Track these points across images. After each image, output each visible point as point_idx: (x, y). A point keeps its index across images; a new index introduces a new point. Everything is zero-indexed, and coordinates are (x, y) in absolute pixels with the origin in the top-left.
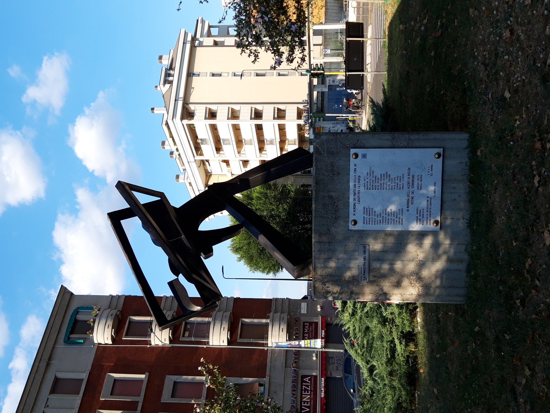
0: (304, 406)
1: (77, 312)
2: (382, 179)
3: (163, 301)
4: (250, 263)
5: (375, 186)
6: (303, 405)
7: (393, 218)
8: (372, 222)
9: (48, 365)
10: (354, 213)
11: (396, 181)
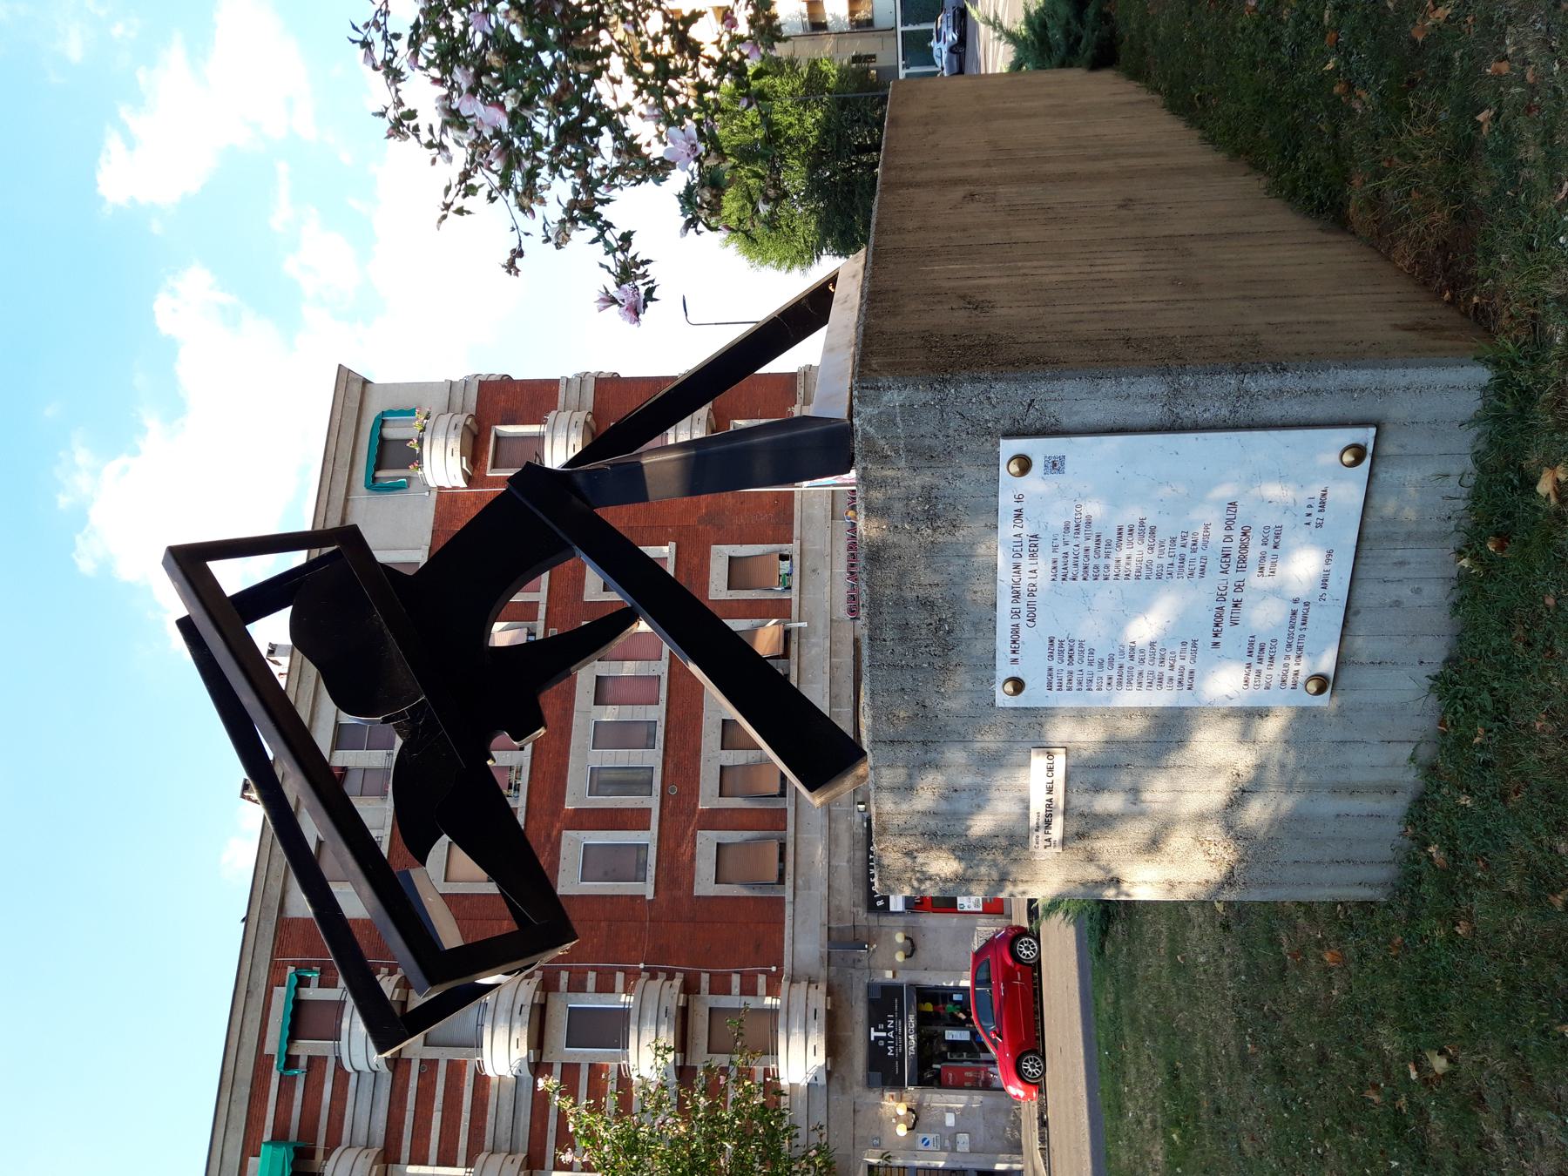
1: (381, 422)
3: (562, 388)
4: (748, 251)
5: (1096, 567)
8: (1080, 683)
10: (1014, 656)
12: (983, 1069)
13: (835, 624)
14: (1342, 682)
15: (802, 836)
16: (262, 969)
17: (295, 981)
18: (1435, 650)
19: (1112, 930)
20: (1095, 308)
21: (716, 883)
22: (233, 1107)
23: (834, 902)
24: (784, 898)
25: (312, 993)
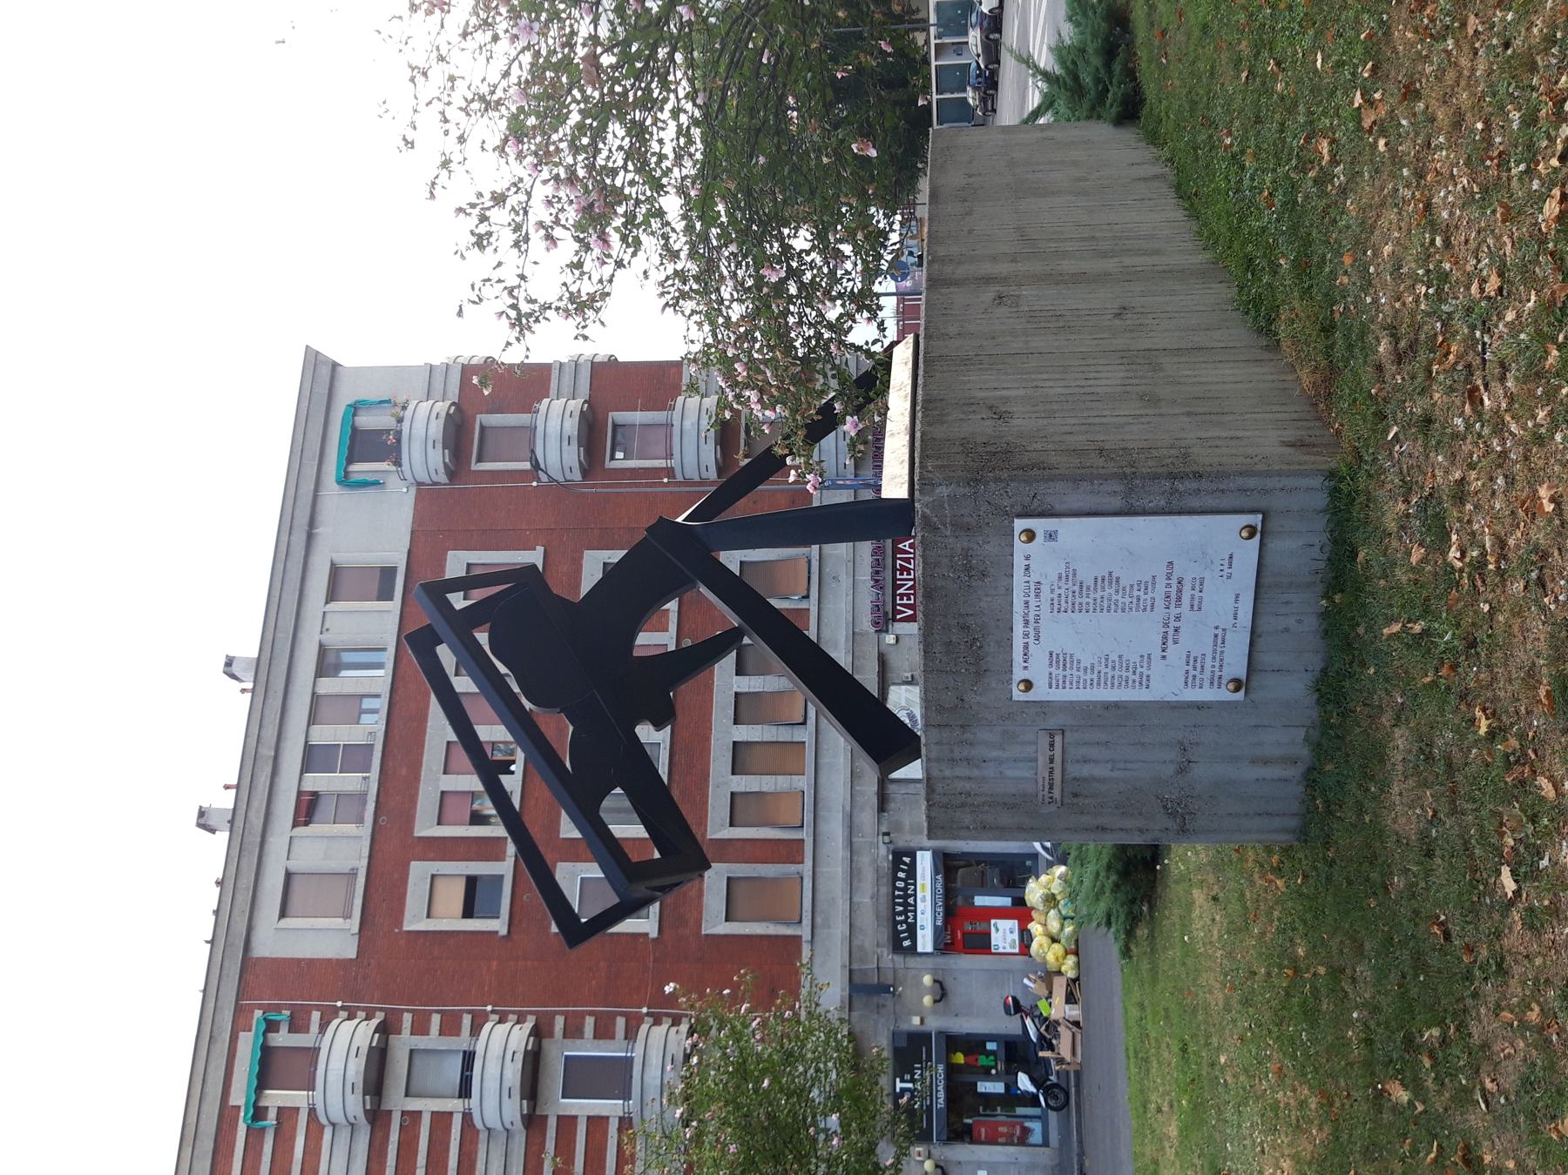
0: (901, 605)
2: (1099, 587)
5: (1081, 604)
6: (898, 602)
7: (1124, 674)
8: (1071, 683)
9: (310, 537)
10: (1026, 665)
11: (1136, 593)
12: (1018, 1123)
13: (857, 637)
14: (1254, 684)
15: (821, 869)
16: (226, 1012)
17: (263, 1027)
18: (1315, 662)
19: (1139, 932)
20: (1083, 421)
21: (727, 920)
22: (195, 1163)
23: (856, 943)
24: (800, 937)
25: (282, 1038)
